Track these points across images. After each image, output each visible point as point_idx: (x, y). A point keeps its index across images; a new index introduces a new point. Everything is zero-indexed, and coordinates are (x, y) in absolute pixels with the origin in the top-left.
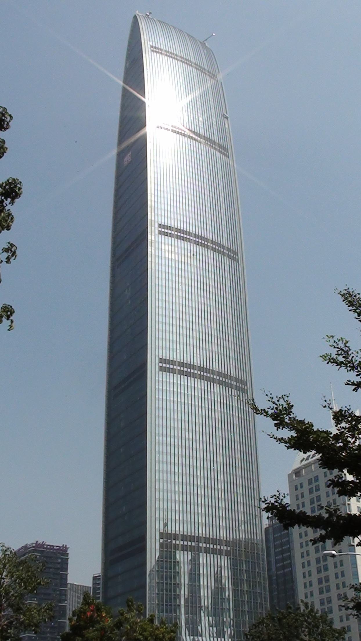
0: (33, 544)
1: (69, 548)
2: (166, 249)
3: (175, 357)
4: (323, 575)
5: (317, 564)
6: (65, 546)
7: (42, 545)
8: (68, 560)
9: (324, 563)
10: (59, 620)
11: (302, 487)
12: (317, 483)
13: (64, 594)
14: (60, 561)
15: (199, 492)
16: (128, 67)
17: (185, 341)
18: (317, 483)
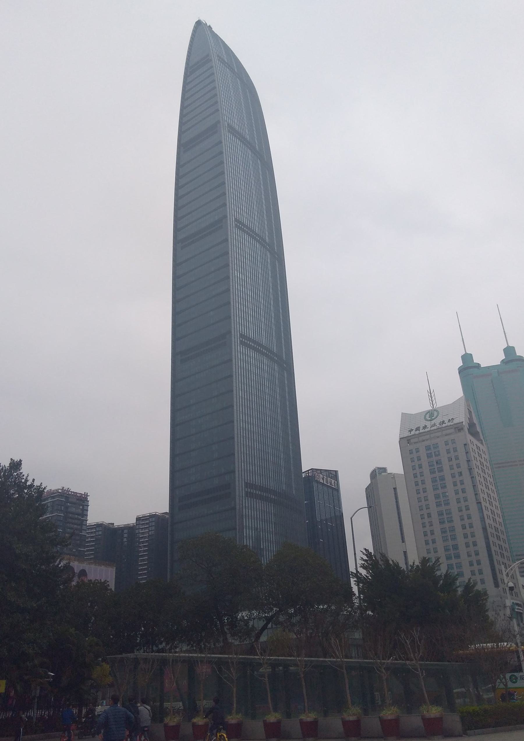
0: (59, 489)
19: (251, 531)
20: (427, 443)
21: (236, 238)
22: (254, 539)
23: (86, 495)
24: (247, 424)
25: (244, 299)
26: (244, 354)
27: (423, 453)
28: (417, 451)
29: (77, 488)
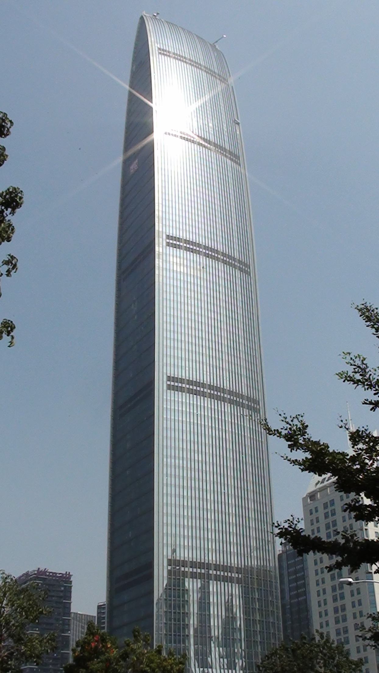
0: (34, 571)
1: (72, 575)
2: (174, 262)
3: (184, 375)
4: (339, 603)
5: (332, 592)
6: (68, 573)
7: (45, 572)
8: (71, 588)
9: (341, 592)
10: (62, 651)
11: (317, 511)
12: (333, 508)
13: (67, 623)
14: (62, 589)
15: (209, 517)
16: (134, 70)
17: (194, 358)
18: (333, 508)
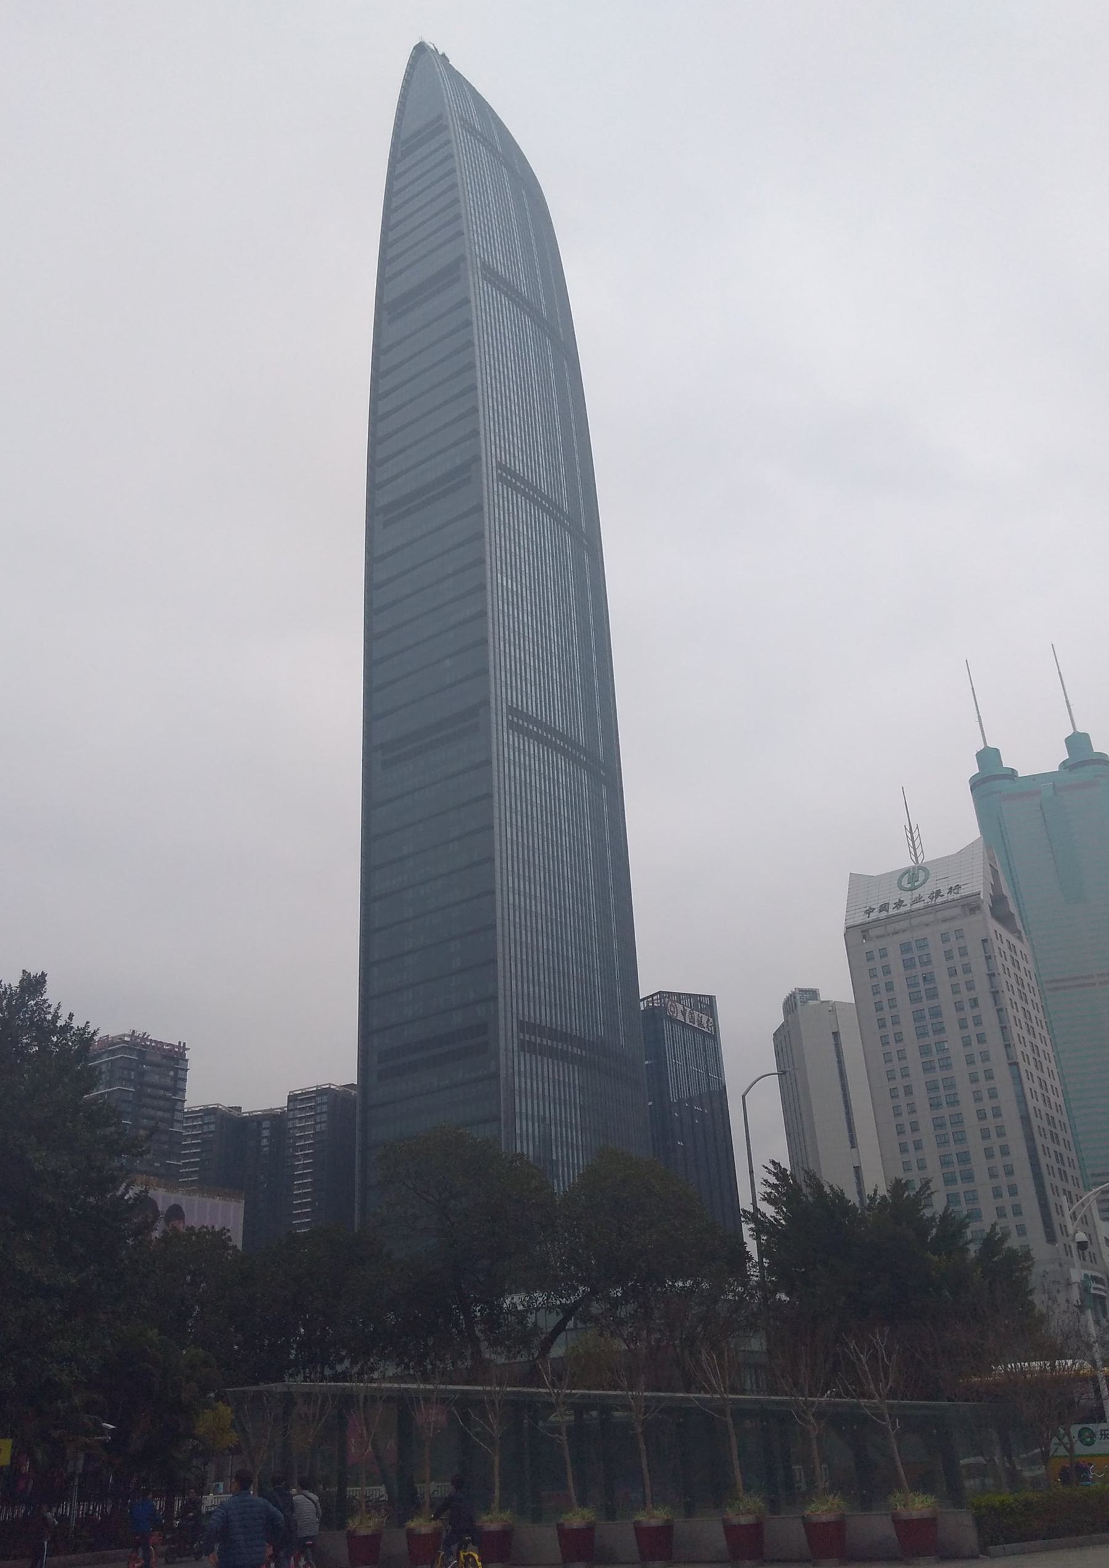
0: (125, 1035)
19: (530, 1124)
20: (903, 938)
21: (499, 503)
22: (537, 1140)
23: (183, 1048)
24: (522, 898)
25: (517, 633)
26: (517, 750)
27: (895, 959)
28: (884, 954)
29: (163, 1033)
